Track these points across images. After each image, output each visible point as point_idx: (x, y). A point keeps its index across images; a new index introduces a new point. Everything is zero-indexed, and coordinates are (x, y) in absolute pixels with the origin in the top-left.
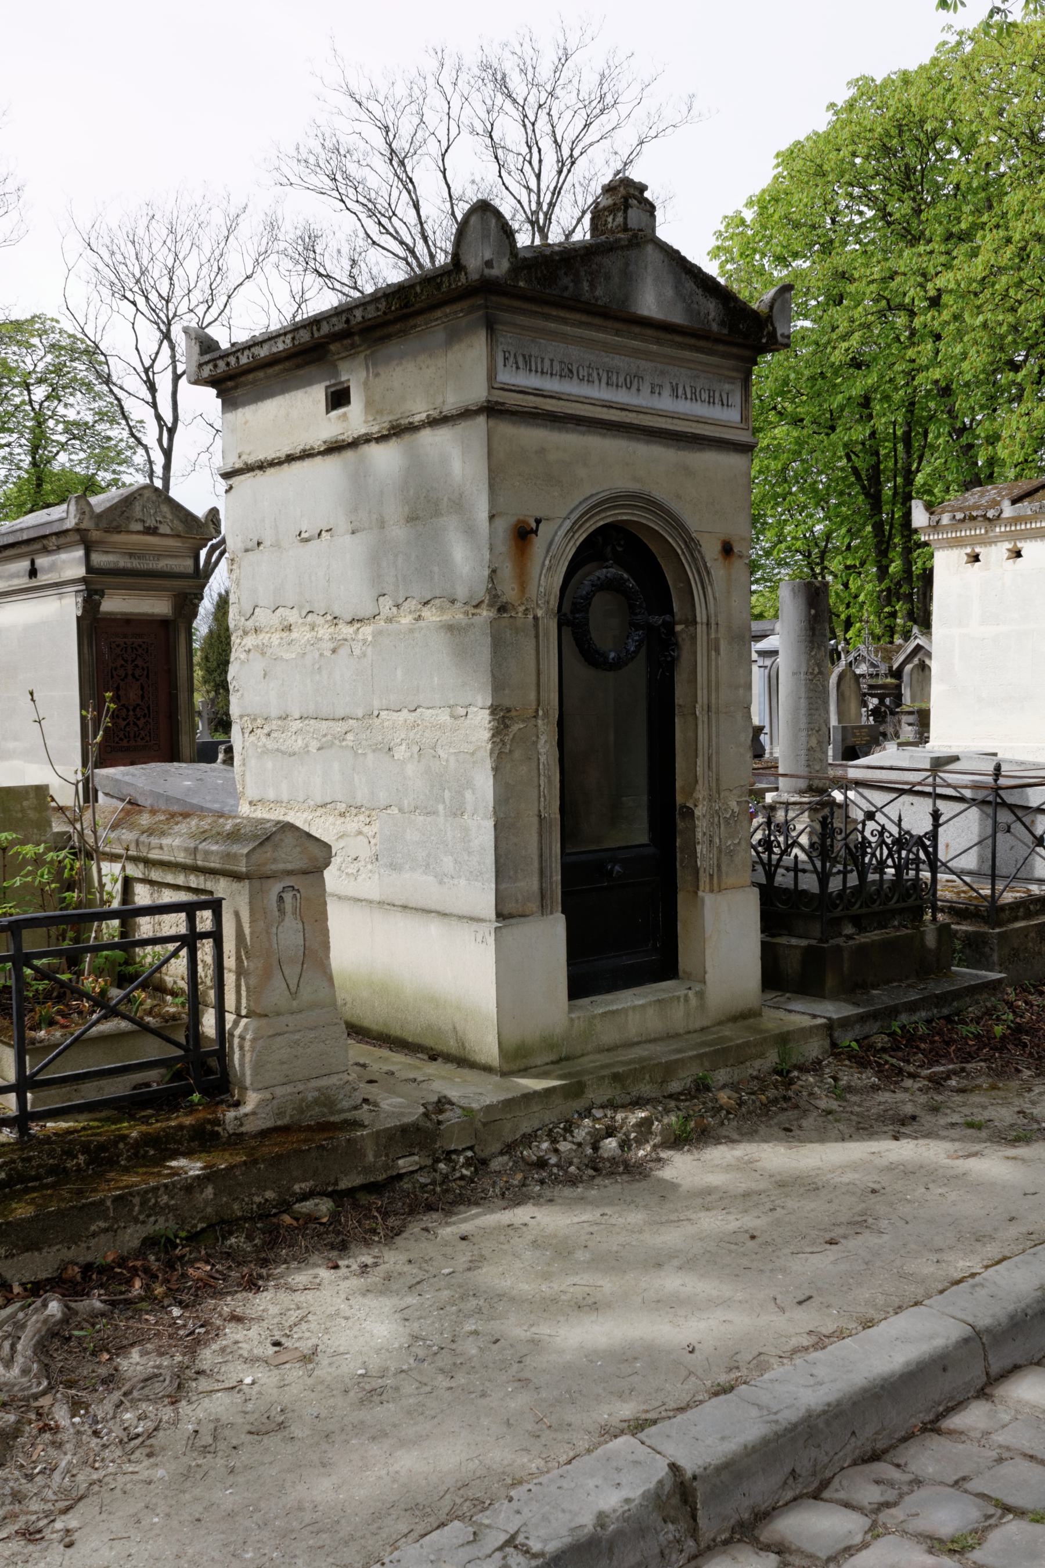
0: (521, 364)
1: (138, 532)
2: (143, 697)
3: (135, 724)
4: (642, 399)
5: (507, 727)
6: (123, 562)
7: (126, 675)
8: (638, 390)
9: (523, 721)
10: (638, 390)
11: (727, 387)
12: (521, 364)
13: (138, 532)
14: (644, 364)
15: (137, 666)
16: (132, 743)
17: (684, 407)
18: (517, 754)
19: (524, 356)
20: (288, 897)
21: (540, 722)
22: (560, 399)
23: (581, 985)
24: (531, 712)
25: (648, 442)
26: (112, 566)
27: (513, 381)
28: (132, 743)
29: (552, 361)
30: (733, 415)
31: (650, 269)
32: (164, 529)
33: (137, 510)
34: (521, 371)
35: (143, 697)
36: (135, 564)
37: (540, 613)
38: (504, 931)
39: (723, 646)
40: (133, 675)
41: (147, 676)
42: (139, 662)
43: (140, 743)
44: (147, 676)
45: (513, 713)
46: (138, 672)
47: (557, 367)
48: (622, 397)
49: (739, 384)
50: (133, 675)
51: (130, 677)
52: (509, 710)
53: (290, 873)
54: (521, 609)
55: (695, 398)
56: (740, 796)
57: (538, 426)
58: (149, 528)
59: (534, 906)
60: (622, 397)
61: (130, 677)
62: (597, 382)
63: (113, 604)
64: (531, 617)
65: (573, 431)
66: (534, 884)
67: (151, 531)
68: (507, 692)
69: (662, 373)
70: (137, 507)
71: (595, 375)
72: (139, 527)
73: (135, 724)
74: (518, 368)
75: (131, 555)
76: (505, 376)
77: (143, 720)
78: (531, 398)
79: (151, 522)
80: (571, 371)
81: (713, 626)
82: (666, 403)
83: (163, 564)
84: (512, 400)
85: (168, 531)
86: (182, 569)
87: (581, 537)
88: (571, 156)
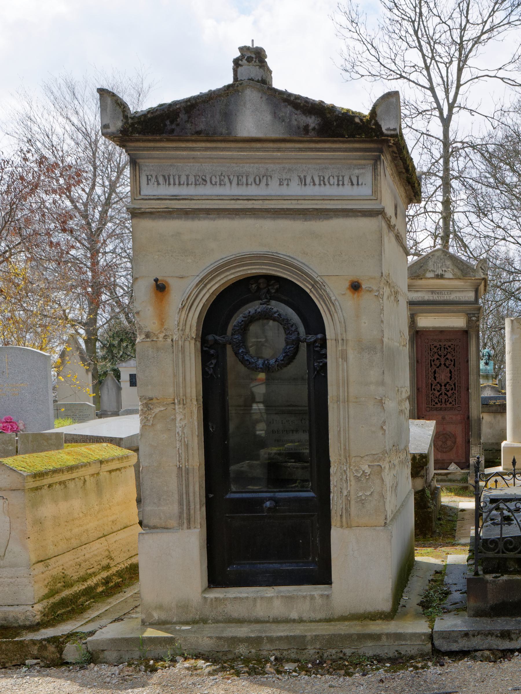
1: (432, 278)
2: (451, 378)
3: (445, 394)
4: (274, 189)
6: (427, 297)
7: (440, 364)
8: (267, 185)
9: (163, 406)
10: (267, 185)
11: (357, 171)
12: (161, 180)
13: (432, 278)
14: (271, 167)
15: (447, 359)
16: (444, 406)
17: (310, 190)
18: (159, 426)
19: (164, 176)
21: (177, 406)
22: (191, 200)
24: (170, 400)
26: (420, 299)
27: (155, 193)
28: (444, 406)
29: (188, 176)
31: (248, 105)
32: (447, 275)
33: (430, 265)
34: (161, 186)
35: (451, 378)
37: (175, 338)
38: (146, 536)
39: (351, 355)
40: (445, 364)
41: (454, 365)
42: (449, 356)
43: (448, 405)
44: (454, 365)
45: (155, 401)
46: (448, 363)
47: (192, 179)
48: (252, 190)
50: (445, 364)
51: (443, 366)
52: (151, 399)
54: (161, 335)
56: (372, 462)
57: (173, 218)
58: (438, 275)
59: (173, 523)
60: (252, 190)
61: (443, 366)
62: (228, 184)
63: (425, 322)
64: (169, 340)
65: (204, 219)
67: (440, 277)
68: (150, 387)
70: (430, 263)
71: (226, 180)
72: (431, 275)
73: (445, 394)
74: (158, 184)
75: (432, 292)
76: (147, 190)
77: (450, 392)
78: (168, 201)
79: (439, 272)
80: (205, 181)
81: (340, 341)
82: (295, 189)
83: (453, 297)
85: (451, 276)
86: (467, 299)
87: (216, 286)
88: (408, 17)
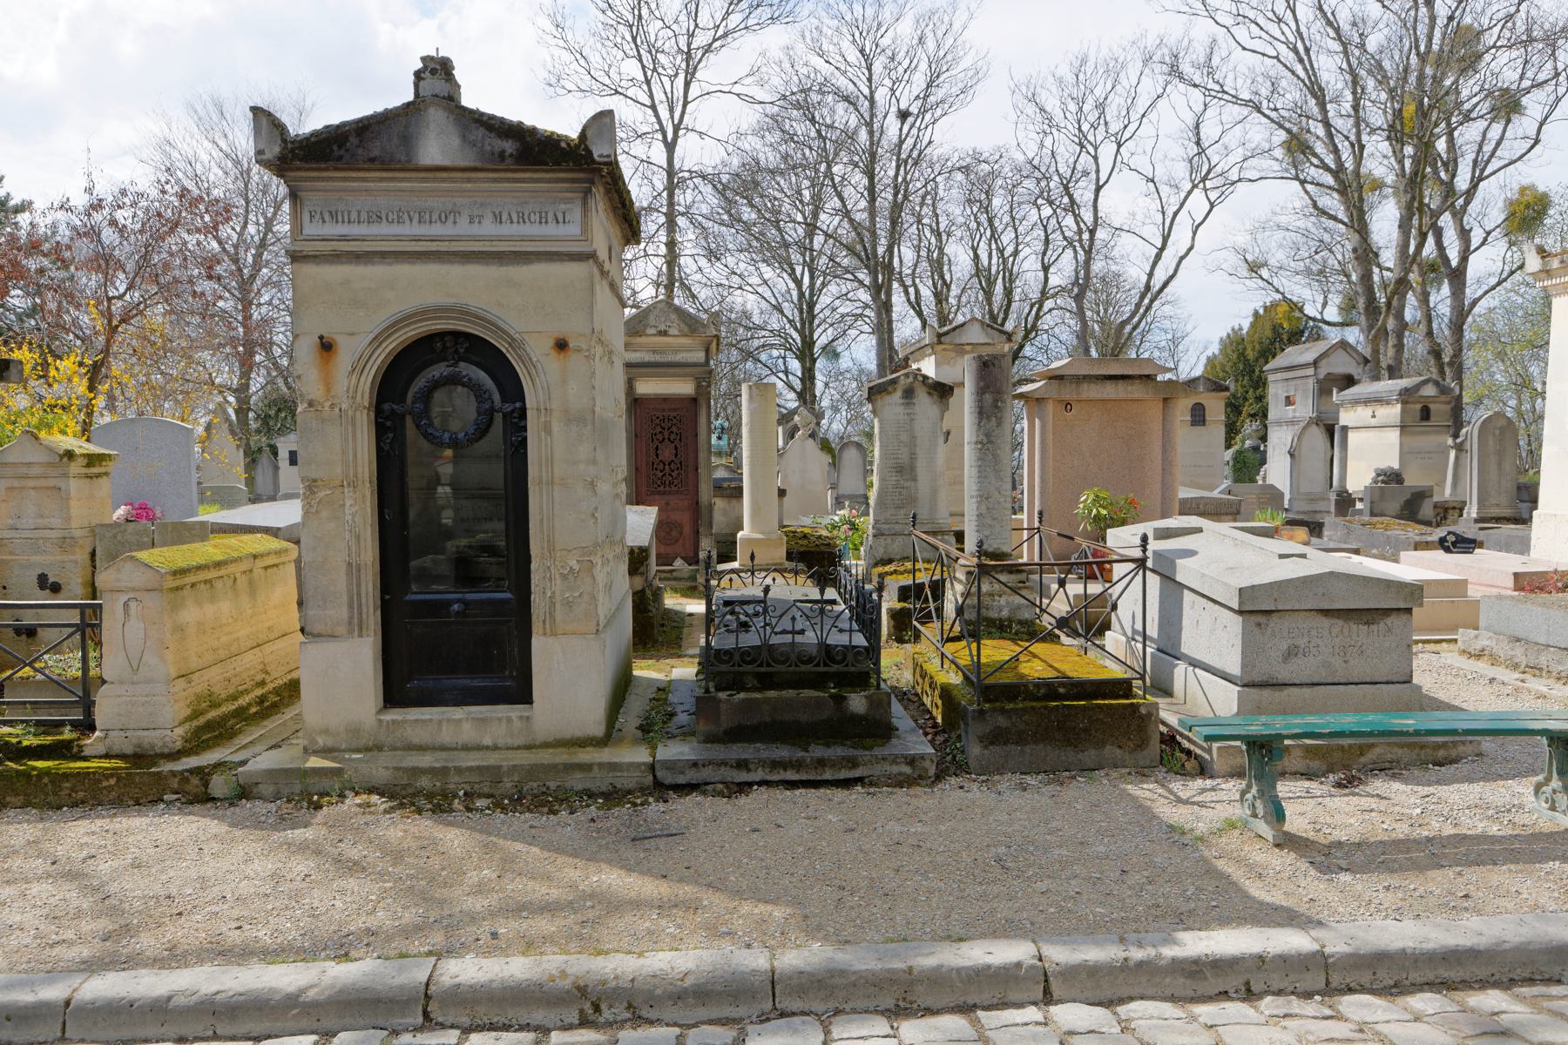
0: (327, 217)
4: (463, 227)
5: (313, 493)
6: (648, 357)
17: (506, 229)
18: (324, 514)
20: (133, 605)
23: (395, 694)
24: (338, 482)
25: (463, 263)
27: (320, 232)
30: (573, 229)
31: (432, 126)
33: (652, 319)
36: (658, 358)
39: (556, 427)
42: (674, 429)
47: (364, 216)
48: (437, 229)
49: (579, 203)
53: (133, 590)
54: (328, 404)
55: (522, 219)
59: (342, 630)
60: (437, 229)
63: (646, 387)
66: (344, 613)
67: (664, 333)
69: (482, 205)
70: (652, 317)
76: (311, 229)
79: (662, 328)
82: (488, 228)
83: (679, 357)
84: (309, 248)
